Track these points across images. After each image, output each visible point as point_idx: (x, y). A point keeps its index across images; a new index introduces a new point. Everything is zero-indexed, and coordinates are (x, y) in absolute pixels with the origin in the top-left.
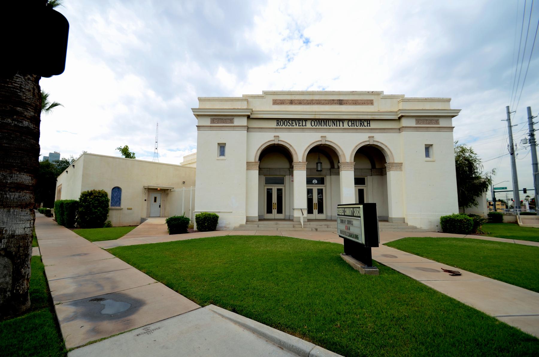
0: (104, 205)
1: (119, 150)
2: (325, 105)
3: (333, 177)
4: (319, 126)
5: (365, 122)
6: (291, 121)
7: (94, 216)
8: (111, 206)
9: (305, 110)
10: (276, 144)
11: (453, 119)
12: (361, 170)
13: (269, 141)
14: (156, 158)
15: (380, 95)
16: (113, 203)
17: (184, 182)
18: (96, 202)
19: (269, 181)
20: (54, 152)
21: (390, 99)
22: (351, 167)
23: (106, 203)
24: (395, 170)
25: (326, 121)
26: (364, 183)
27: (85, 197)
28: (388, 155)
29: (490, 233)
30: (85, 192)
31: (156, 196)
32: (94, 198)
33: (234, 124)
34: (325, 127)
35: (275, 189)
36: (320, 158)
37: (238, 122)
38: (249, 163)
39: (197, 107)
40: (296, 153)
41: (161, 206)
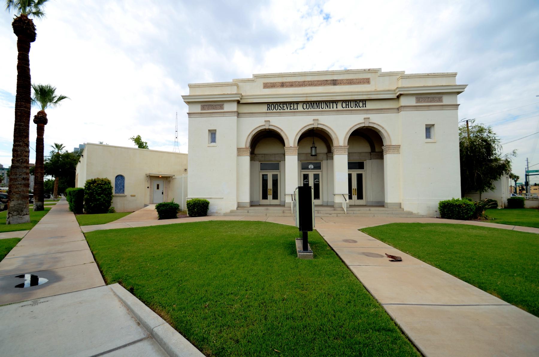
0: (107, 193)
1: (132, 140)
2: (318, 86)
3: (329, 161)
4: (311, 109)
5: (360, 102)
7: (98, 202)
8: (115, 193)
9: (296, 92)
10: (267, 129)
12: (359, 154)
13: (259, 127)
14: (177, 147)
15: (378, 72)
16: (117, 191)
17: (186, 169)
20: (84, 143)
22: (345, 150)
23: (109, 190)
24: (392, 153)
25: (319, 103)
27: (88, 184)
28: (385, 137)
29: (495, 219)
30: (90, 180)
32: (97, 185)
33: (224, 109)
34: (318, 110)
35: (355, 173)
37: (228, 107)
38: (240, 149)
40: (287, 138)
41: (164, 193)
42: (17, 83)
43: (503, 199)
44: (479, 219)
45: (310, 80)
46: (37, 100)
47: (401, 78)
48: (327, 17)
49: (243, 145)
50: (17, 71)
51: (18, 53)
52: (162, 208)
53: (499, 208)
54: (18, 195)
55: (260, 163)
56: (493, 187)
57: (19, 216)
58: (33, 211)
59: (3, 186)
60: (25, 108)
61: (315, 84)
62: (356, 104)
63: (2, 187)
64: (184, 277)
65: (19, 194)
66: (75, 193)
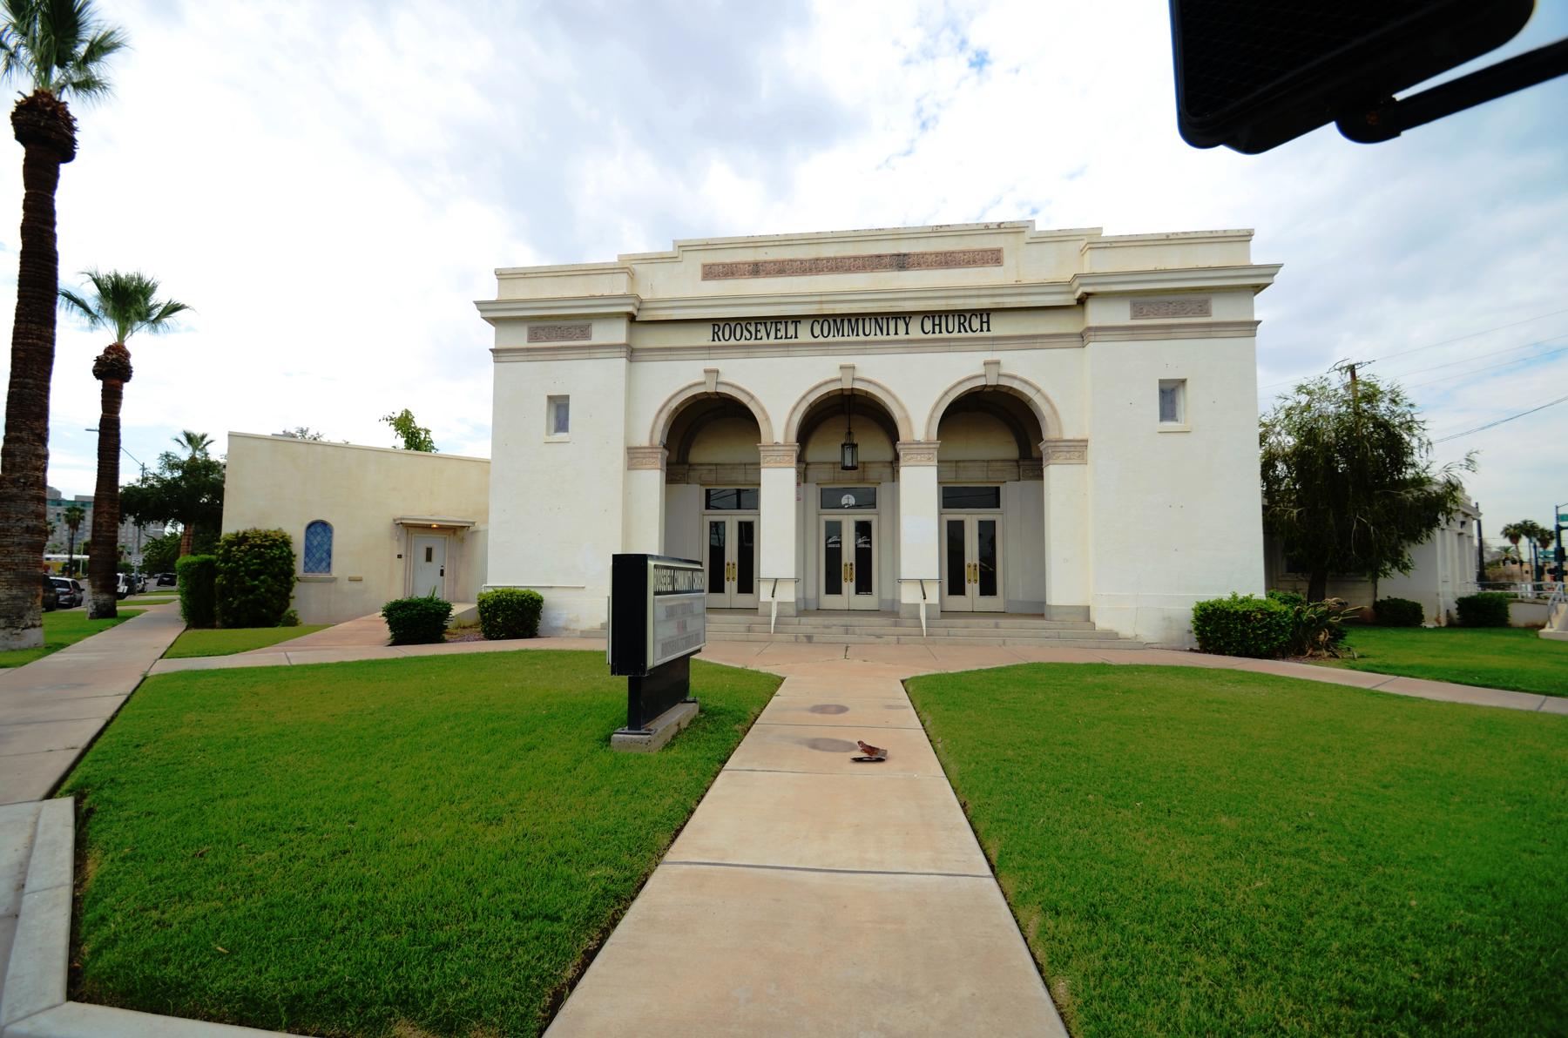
0: (277, 570)
1: (389, 422)
2: (854, 272)
5: (974, 317)
6: (753, 326)
8: (305, 572)
10: (712, 394)
11: (1257, 298)
12: (986, 464)
13: (690, 387)
16: (310, 564)
18: (255, 561)
19: (829, 500)
23: (283, 564)
24: (1066, 462)
25: (857, 321)
26: (873, 505)
30: (231, 534)
31: (429, 546)
32: (249, 550)
34: (853, 338)
35: (971, 520)
36: (852, 430)
38: (635, 451)
41: (445, 572)
42: (20, 271)
43: (1441, 599)
44: (1311, 655)
45: (832, 255)
46: (106, 314)
47: (1090, 248)
48: (980, 61)
49: (643, 439)
50: (20, 241)
51: (25, 191)
52: (399, 614)
53: (1429, 624)
54: (12, 572)
55: (703, 490)
56: (1406, 564)
57: (11, 629)
58: (87, 619)
59: (56, 550)
60: (37, 339)
61: (847, 265)
62: (716, 330)
63: (54, 553)
64: (165, 763)
65: (14, 569)
66: (190, 569)
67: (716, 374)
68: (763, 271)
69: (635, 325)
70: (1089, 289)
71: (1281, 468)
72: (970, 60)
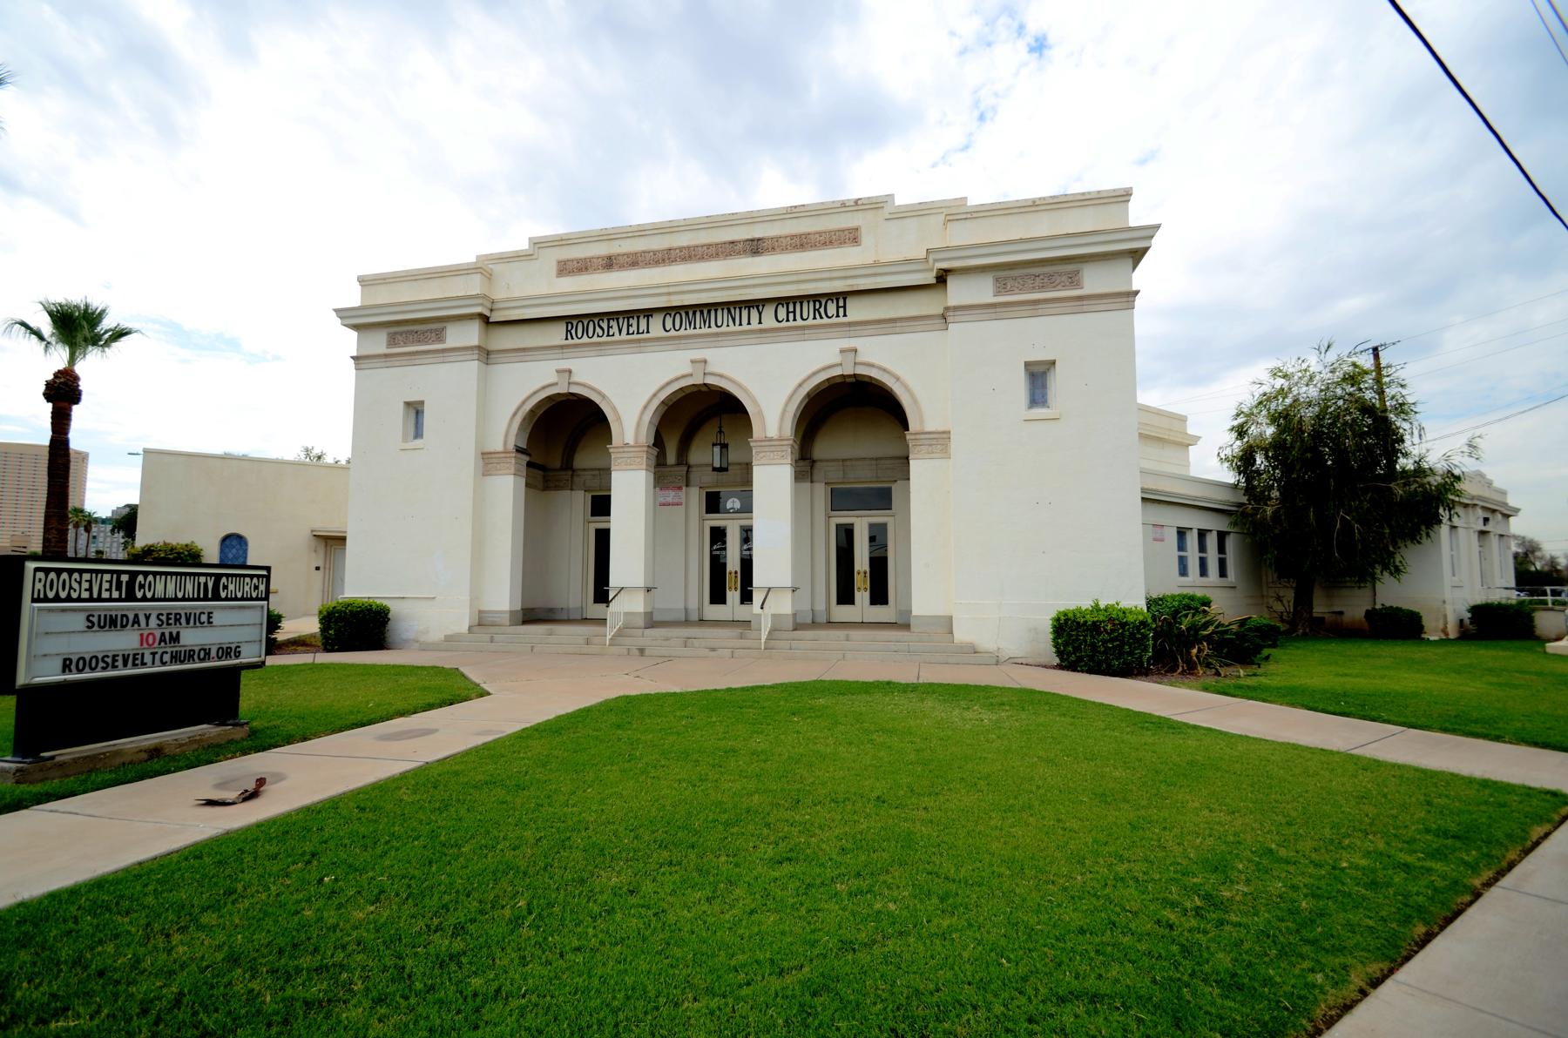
2: (707, 260)
4: (728, 326)
6: (606, 321)
12: (874, 462)
13: (544, 388)
15: (883, 207)
19: (841, 499)
21: (915, 219)
22: (783, 451)
25: (709, 312)
34: (705, 330)
35: (861, 524)
38: (489, 456)
39: (355, 301)
45: (685, 244)
48: (1039, 46)
49: (496, 444)
62: (817, 307)
67: (567, 374)
68: (617, 264)
69: (491, 327)
70: (945, 265)
71: (1259, 459)
72: (1028, 45)
